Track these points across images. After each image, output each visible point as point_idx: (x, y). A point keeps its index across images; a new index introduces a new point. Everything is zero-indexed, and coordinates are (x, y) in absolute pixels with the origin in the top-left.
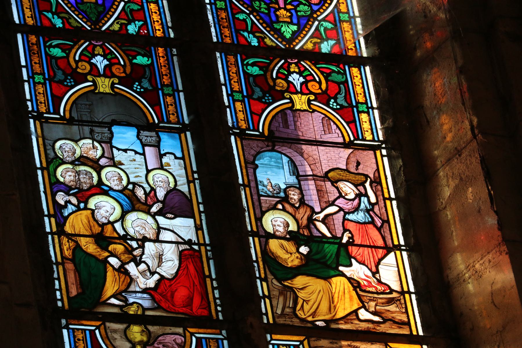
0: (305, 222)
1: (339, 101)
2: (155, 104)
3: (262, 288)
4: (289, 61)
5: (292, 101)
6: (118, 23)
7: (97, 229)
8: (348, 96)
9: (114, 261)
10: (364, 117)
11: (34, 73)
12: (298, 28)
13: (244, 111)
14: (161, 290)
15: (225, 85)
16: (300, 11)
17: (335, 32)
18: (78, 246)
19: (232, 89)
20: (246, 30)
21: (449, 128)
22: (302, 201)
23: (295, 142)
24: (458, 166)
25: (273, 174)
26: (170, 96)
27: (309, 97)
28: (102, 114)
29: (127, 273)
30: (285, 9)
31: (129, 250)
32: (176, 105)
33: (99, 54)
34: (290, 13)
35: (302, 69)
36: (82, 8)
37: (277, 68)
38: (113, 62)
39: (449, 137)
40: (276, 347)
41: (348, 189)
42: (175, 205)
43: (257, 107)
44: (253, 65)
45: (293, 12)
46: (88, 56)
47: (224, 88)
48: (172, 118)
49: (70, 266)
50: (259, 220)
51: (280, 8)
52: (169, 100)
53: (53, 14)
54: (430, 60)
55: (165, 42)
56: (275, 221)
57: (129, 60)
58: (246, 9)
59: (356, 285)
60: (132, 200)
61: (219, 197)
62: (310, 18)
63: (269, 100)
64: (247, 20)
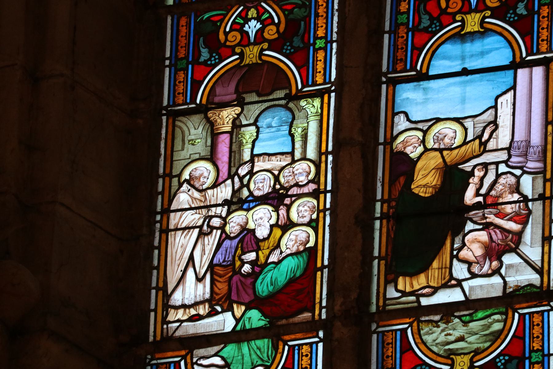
1: (295, 44)
4: (248, 5)
8: (306, 36)
32: (327, 62)
33: (252, 18)
35: (261, 11)
37: (274, 14)
40: (154, 367)
63: (287, 49)
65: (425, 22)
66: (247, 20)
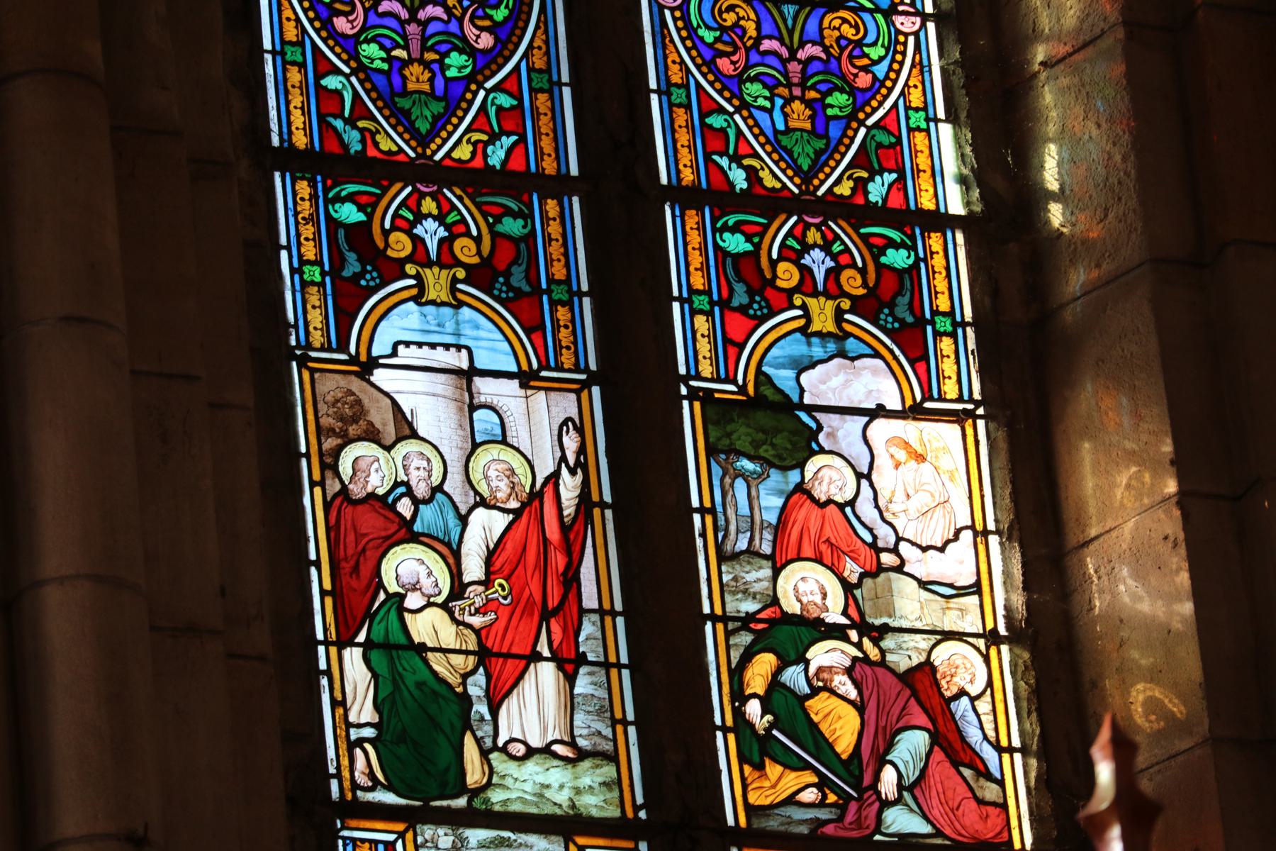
4: (422, 188)
5: (807, 315)
6: (849, 178)
8: (533, 272)
11: (303, 262)
12: (446, 108)
13: (712, 337)
15: (288, 248)
16: (832, 106)
19: (300, 256)
20: (340, 115)
26: (563, 306)
27: (838, 305)
30: (421, 61)
34: (431, 71)
35: (446, 207)
36: (783, 143)
38: (456, 230)
44: (735, 229)
45: (435, 67)
47: (284, 255)
48: (567, 359)
51: (410, 61)
52: (562, 313)
53: (346, 121)
57: (872, 253)
58: (729, 101)
64: (345, 93)
65: (740, 298)
66: (420, 217)
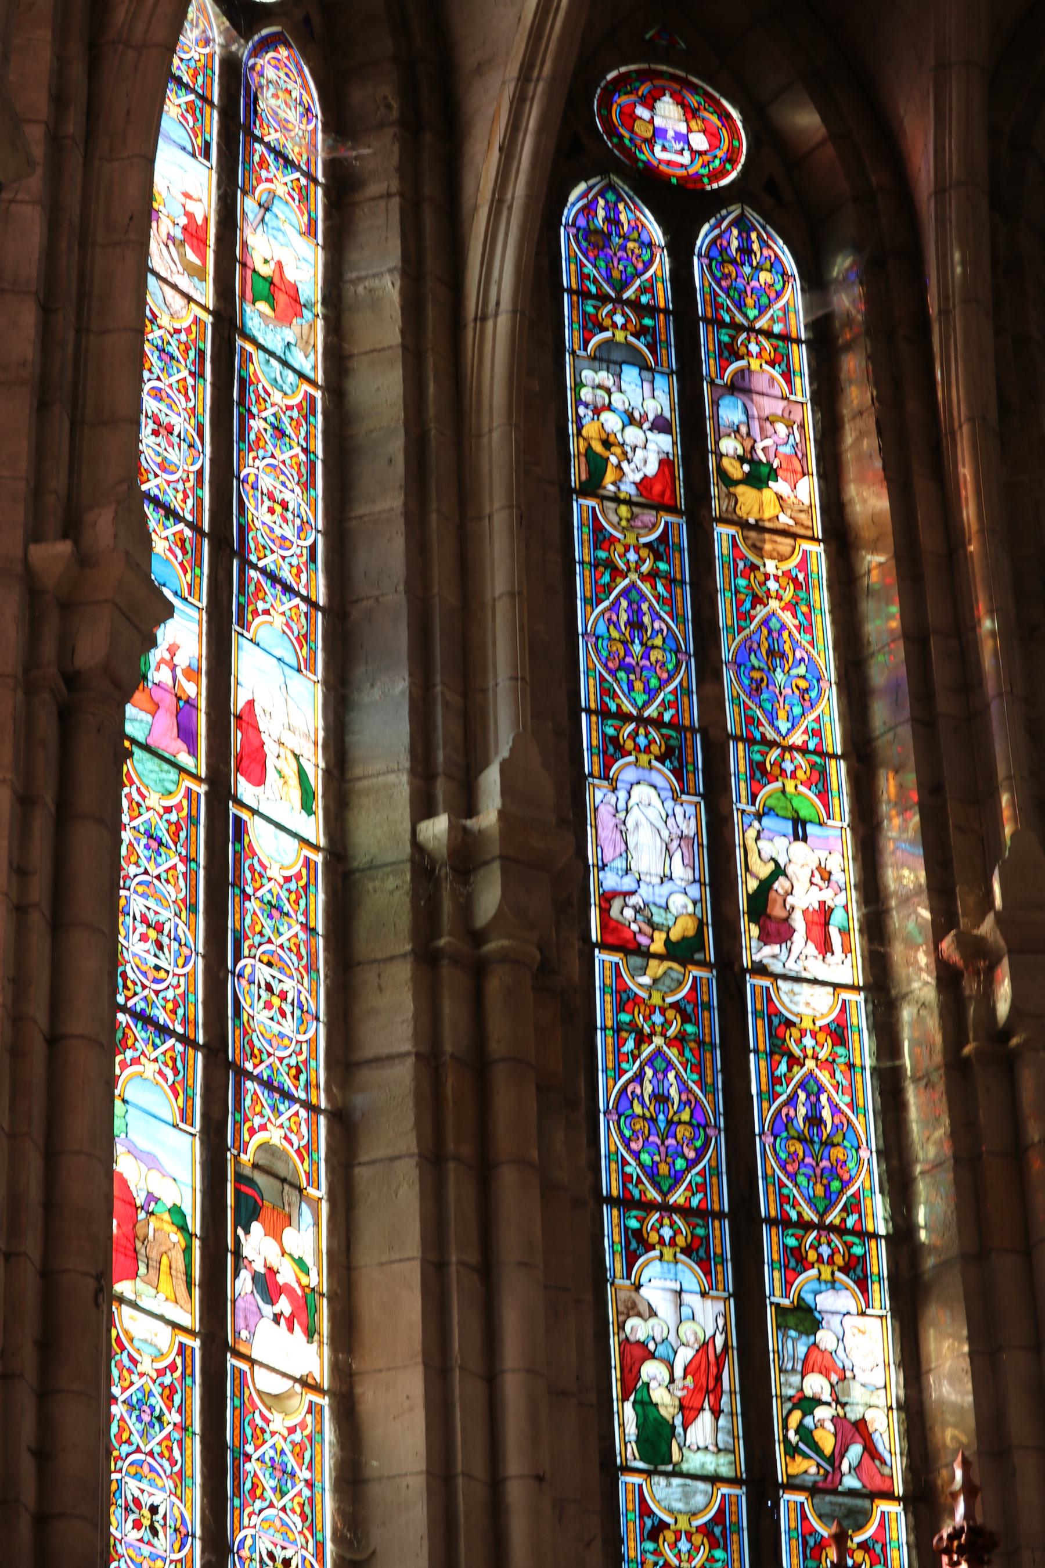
0: (749, 448)
2: (654, 352)
3: (714, 491)
7: (604, 436)
9: (613, 460)
10: (776, 1257)
14: (643, 485)
17: (785, 319)
18: (589, 447)
21: (857, 396)
22: (749, 434)
23: (748, 392)
24: (860, 423)
25: (731, 412)
28: (616, 356)
29: (621, 469)
31: (625, 453)
39: (855, 402)
41: (781, 429)
42: (661, 425)
43: (724, 364)
46: (611, 314)
49: (583, 459)
50: (717, 443)
54: (848, 347)
55: (666, 311)
56: (729, 446)
59: (780, 498)
60: (630, 419)
61: (692, 424)
62: (769, 306)
